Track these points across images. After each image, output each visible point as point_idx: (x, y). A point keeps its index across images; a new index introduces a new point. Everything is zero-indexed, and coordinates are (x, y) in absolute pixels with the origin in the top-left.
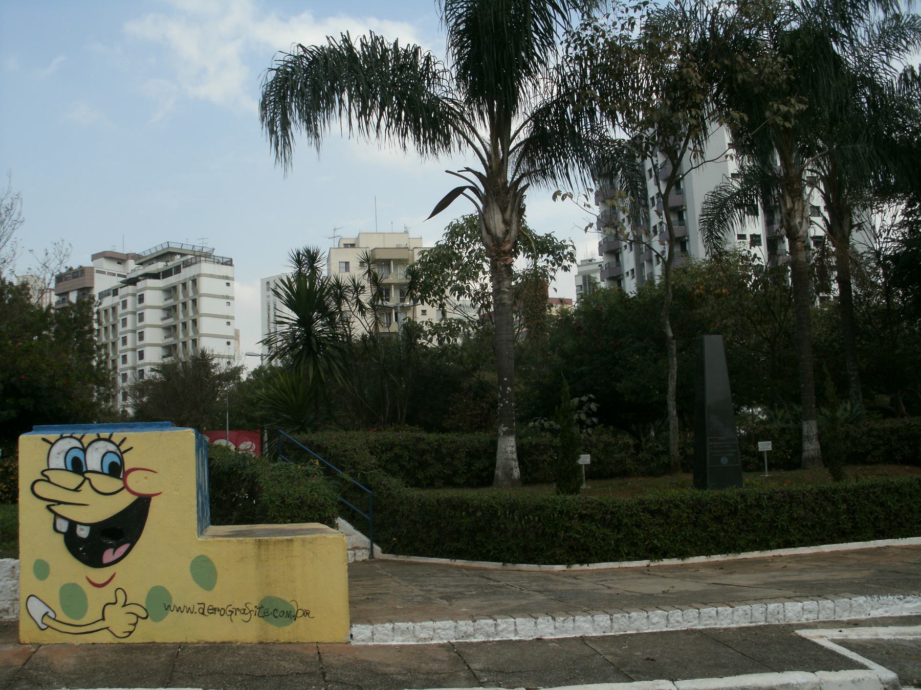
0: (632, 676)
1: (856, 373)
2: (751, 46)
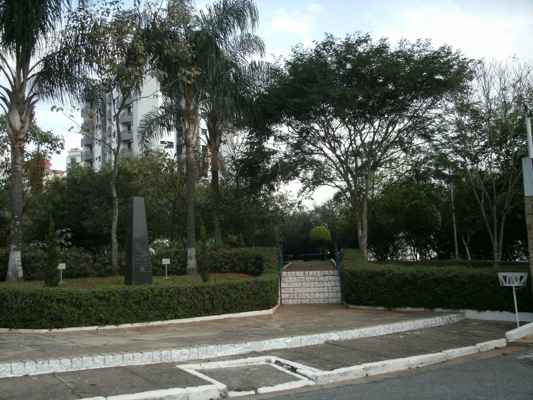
0: (82, 395)
1: (218, 222)
2: (174, 36)
